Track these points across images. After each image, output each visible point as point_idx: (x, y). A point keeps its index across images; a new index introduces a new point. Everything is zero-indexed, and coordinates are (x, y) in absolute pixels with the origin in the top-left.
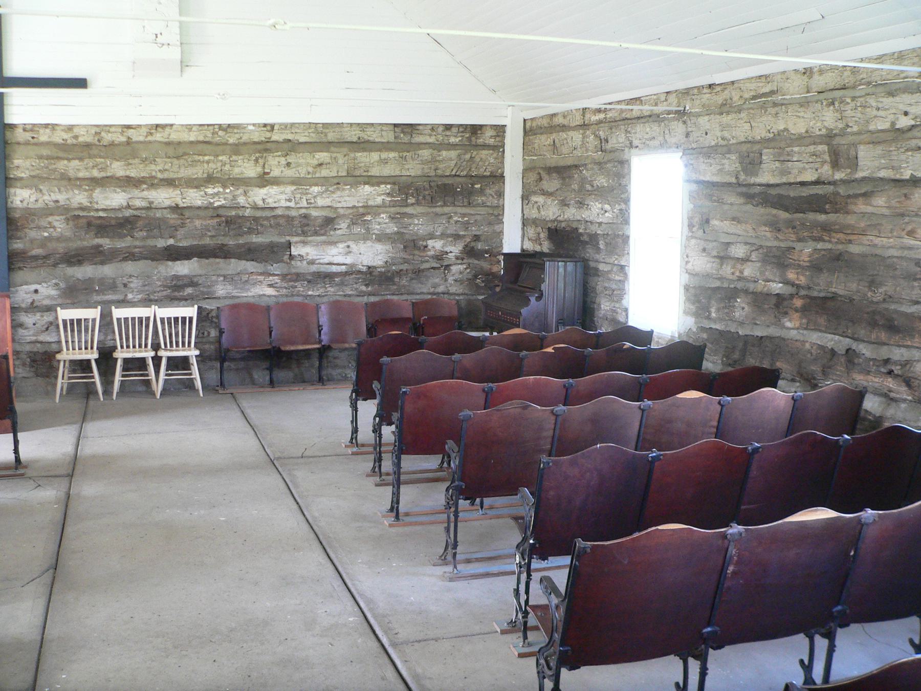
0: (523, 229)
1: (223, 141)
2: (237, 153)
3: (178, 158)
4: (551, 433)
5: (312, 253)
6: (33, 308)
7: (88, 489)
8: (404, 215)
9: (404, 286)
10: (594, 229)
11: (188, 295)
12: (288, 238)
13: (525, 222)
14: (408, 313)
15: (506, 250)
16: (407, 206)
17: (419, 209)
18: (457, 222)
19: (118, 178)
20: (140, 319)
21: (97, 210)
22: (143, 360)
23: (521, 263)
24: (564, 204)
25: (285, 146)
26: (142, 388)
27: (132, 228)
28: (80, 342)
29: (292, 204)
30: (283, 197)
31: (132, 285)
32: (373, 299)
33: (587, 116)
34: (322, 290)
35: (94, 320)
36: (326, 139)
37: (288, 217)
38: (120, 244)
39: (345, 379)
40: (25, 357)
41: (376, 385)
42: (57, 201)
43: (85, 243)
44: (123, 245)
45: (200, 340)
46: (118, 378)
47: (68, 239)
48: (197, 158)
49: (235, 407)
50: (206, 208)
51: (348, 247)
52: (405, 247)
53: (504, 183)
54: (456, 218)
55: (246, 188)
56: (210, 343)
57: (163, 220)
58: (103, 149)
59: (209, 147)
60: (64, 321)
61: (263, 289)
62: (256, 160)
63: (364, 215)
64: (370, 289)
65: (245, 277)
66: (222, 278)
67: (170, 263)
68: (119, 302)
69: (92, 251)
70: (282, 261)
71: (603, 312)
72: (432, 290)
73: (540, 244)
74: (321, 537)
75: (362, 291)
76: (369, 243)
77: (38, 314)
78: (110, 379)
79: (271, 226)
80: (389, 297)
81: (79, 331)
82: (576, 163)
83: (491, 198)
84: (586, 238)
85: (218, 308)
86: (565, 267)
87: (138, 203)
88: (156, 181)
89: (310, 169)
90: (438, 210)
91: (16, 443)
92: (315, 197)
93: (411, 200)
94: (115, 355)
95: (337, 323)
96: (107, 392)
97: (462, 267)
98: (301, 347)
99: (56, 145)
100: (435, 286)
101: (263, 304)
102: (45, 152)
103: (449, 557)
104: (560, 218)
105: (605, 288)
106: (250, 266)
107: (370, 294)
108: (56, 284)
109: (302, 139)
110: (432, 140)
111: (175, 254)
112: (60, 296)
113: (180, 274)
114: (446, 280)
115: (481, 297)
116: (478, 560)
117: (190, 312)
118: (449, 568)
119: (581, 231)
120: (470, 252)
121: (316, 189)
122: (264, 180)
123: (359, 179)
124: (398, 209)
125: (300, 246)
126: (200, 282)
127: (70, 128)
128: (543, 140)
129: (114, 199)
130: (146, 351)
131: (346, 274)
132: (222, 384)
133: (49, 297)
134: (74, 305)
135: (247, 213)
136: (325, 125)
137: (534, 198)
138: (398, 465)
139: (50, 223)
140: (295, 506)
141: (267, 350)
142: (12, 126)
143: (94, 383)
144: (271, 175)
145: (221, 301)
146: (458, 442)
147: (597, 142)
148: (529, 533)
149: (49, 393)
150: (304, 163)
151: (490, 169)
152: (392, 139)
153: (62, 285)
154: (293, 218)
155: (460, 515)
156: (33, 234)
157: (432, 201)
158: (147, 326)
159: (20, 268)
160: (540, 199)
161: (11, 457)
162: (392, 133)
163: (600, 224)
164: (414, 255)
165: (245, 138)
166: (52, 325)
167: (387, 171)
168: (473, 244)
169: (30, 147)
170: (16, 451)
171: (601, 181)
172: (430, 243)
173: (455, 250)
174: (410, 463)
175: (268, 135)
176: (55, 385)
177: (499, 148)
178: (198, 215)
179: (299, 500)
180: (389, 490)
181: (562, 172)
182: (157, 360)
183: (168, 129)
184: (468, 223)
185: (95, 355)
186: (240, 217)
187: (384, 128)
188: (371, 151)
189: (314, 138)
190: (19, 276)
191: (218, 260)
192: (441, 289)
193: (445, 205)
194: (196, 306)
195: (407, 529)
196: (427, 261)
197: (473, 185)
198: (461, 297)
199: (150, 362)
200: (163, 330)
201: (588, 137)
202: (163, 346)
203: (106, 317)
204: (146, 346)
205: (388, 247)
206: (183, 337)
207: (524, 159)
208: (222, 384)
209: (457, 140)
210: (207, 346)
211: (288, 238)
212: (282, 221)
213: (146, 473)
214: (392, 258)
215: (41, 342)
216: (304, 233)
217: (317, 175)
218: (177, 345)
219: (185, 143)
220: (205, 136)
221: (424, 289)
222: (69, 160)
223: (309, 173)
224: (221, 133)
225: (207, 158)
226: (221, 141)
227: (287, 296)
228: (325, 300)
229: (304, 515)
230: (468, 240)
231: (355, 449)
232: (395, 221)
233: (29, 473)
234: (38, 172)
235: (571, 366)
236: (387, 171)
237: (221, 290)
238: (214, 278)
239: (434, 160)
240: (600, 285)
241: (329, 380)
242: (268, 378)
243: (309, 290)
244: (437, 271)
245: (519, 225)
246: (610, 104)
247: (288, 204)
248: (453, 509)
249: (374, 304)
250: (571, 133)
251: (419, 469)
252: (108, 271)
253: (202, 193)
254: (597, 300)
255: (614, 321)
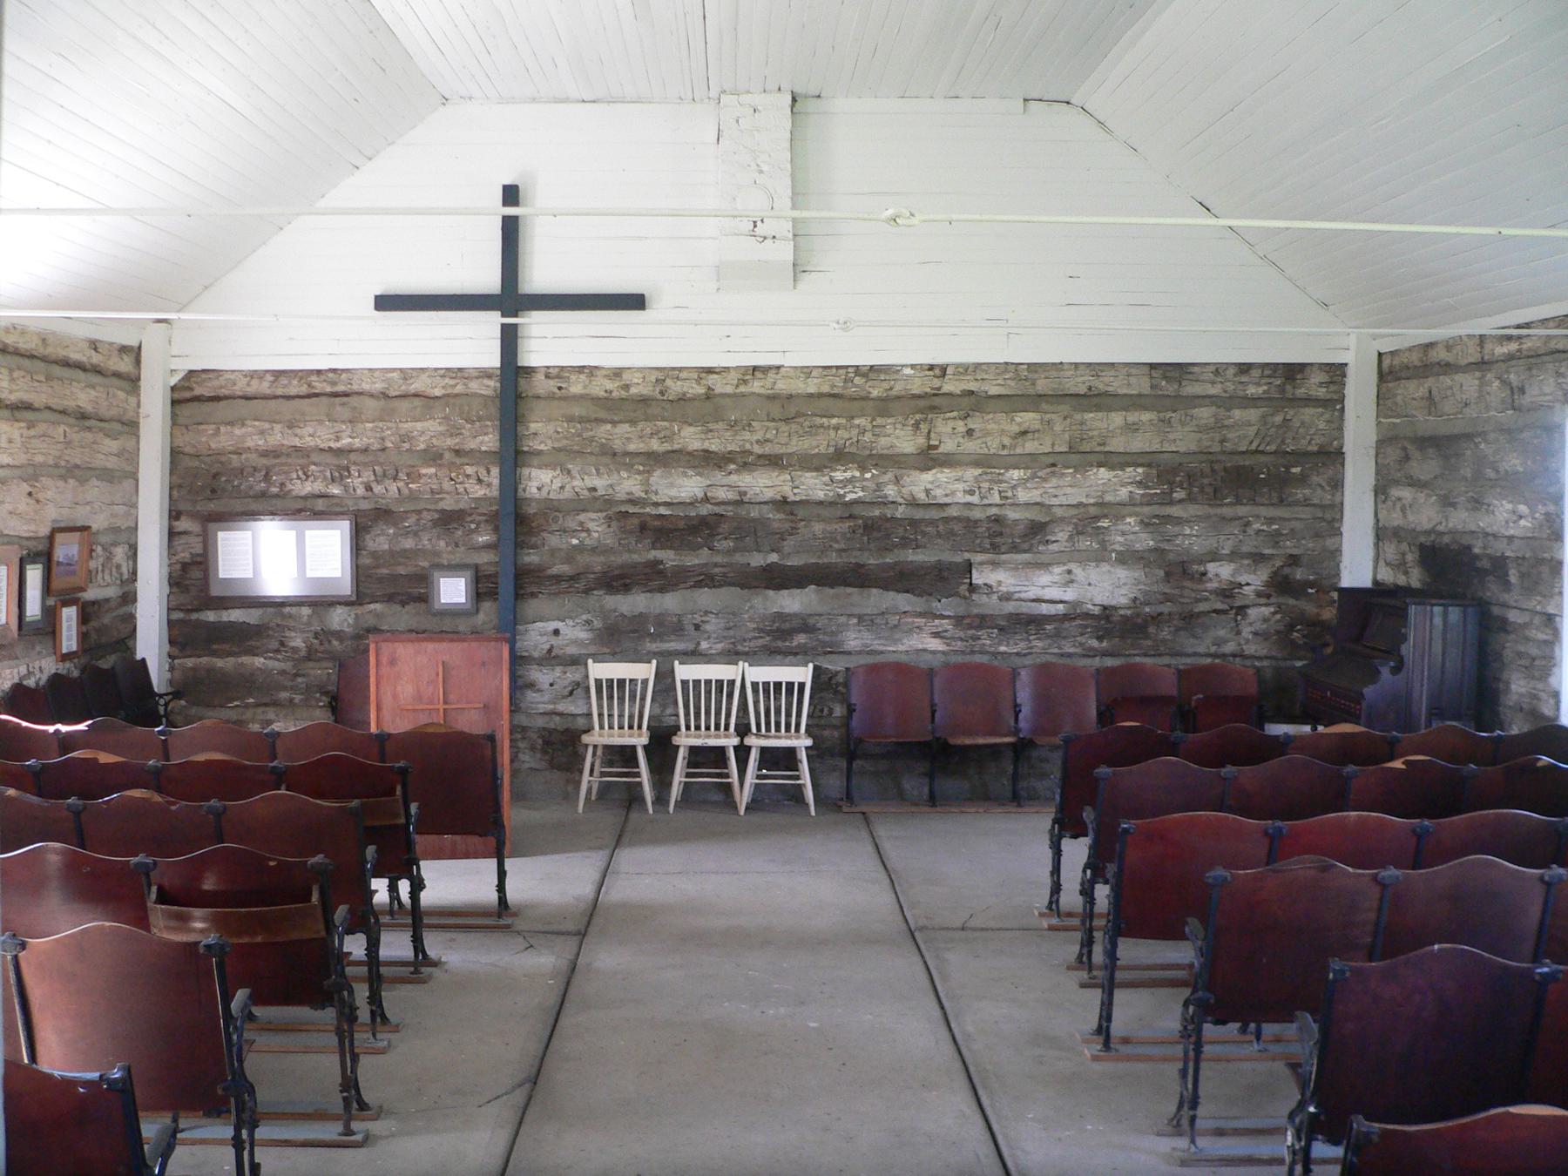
0: (1376, 545)
1: (863, 394)
2: (884, 413)
3: (786, 420)
4: (1372, 916)
5: (1000, 580)
6: (551, 658)
7: (605, 958)
8: (1168, 519)
9: (1164, 641)
10: (1499, 548)
11: (799, 646)
12: (967, 556)
13: (1381, 534)
14: (1169, 687)
15: (1346, 582)
16: (1172, 503)
17: (1193, 510)
18: (1259, 531)
19: (690, 454)
20: (720, 683)
21: (656, 504)
22: (722, 750)
23: (1375, 609)
24: (1447, 502)
25: (966, 401)
26: (718, 797)
27: (712, 535)
28: (621, 716)
29: (975, 499)
30: (960, 486)
31: (708, 627)
32: (1110, 662)
33: (1488, 346)
34: (1022, 645)
35: (645, 682)
36: (1034, 390)
37: (968, 519)
38: (696, 559)
39: (1049, 800)
40: (534, 736)
41: (1088, 815)
42: (594, 489)
43: (636, 558)
44: (697, 562)
45: (815, 721)
46: (678, 777)
47: (607, 551)
48: (818, 421)
49: (864, 834)
50: (832, 504)
51: (1069, 572)
52: (1167, 574)
53: (1343, 465)
54: (1257, 526)
55: (898, 472)
56: (835, 727)
57: (763, 522)
58: (668, 406)
59: (840, 403)
60: (598, 682)
61: (924, 641)
62: (916, 426)
63: (1097, 518)
64: (1105, 644)
65: (894, 620)
66: (855, 621)
67: (771, 593)
68: (685, 653)
69: (648, 570)
70: (957, 594)
71: (1515, 697)
72: (1213, 649)
73: (1406, 573)
74: (972, 1069)
75: (1091, 649)
76: (1105, 567)
77: (559, 669)
78: (670, 783)
79: (939, 535)
80: (1138, 659)
81: (621, 699)
82: (1469, 430)
83: (1319, 491)
84: (1485, 564)
85: (848, 669)
86: (1445, 615)
87: (722, 494)
88: (751, 459)
89: (1007, 441)
90: (1227, 511)
91: (502, 874)
92: (1014, 487)
93: (1179, 494)
94: (676, 740)
95: (1044, 700)
96: (661, 800)
97: (1266, 611)
98: (981, 741)
99: (596, 400)
100: (1219, 642)
101: (922, 665)
102: (577, 411)
103: (1185, 1123)
104: (1441, 528)
105: (1520, 655)
106: (903, 601)
107: (1105, 654)
108: (588, 622)
109: (994, 391)
110: (1213, 391)
111: (778, 578)
112: (593, 641)
113: (786, 611)
114: (1239, 633)
115: (1299, 664)
116: (1237, 1132)
117: (801, 674)
118: (1183, 1143)
119: (1476, 551)
120: (1281, 585)
121: (1016, 474)
122: (929, 458)
123: (1090, 458)
124: (1156, 510)
125: (987, 568)
126: (819, 625)
127: (617, 373)
128: (1413, 390)
129: (685, 487)
130: (726, 736)
131: (1065, 617)
132: (849, 797)
133: (575, 642)
134: (616, 656)
135: (900, 512)
136: (1032, 367)
137: (1395, 492)
138: (1111, 954)
139: (581, 524)
140: (937, 1013)
141: (925, 743)
142: (530, 371)
143: (640, 784)
144: (940, 450)
145: (853, 658)
146: (1204, 921)
147: (1505, 393)
148: (1308, 1094)
149: (570, 797)
150: (995, 431)
151: (1318, 440)
152: (1147, 391)
153: (597, 624)
154: (976, 522)
155: (1207, 1049)
156: (554, 541)
157: (1216, 496)
158: (730, 695)
159: (533, 595)
160: (1406, 493)
161: (493, 896)
162: (1147, 379)
163: (1511, 538)
164: (1183, 588)
165: (898, 388)
166: (579, 688)
167: (1138, 444)
168: (1287, 571)
169: (556, 403)
170: (501, 888)
171: (1513, 462)
172: (1212, 567)
173: (1255, 580)
174: (1133, 951)
175: (936, 383)
176: (579, 783)
177: (1334, 403)
178: (819, 516)
179: (944, 1001)
180: (1096, 996)
181: (1443, 445)
182: (742, 752)
183: (771, 375)
184: (1278, 533)
185: (645, 740)
186: (888, 520)
187: (1133, 371)
188: (1110, 409)
189: (1011, 388)
190: (532, 607)
191: (849, 590)
192: (1230, 648)
193: (1238, 502)
194: (811, 666)
195: (1122, 1067)
196: (1206, 599)
197: (1288, 468)
198: (1266, 663)
199: (732, 754)
200: (756, 703)
201: (1490, 384)
202: (754, 730)
203: (665, 677)
204: (727, 728)
205: (1138, 574)
206: (788, 715)
207: (1379, 424)
208: (849, 797)
209: (1260, 390)
210: (826, 733)
211: (967, 556)
212: (957, 527)
213: (698, 939)
214: (1146, 593)
215: (561, 714)
216: (995, 548)
217: (1019, 451)
218: (778, 729)
219: (798, 396)
220: (833, 386)
221: (1201, 648)
222: (614, 423)
223: (1004, 447)
224: (858, 380)
225: (834, 421)
226: (859, 393)
227: (963, 652)
228: (1028, 661)
229: (950, 1029)
230: (1278, 563)
231: (1055, 921)
232: (1151, 529)
233: (519, 924)
234: (565, 442)
235: (1433, 796)
236: (1138, 444)
237: (854, 639)
238: (842, 619)
239: (1219, 426)
240: (1510, 647)
241: (1030, 798)
242: (926, 790)
243: (1000, 644)
244: (1223, 617)
245: (1370, 539)
246: (1518, 327)
247: (969, 499)
248: (1193, 1039)
249: (1112, 671)
250: (1459, 377)
251: (1159, 961)
252: (670, 602)
253: (826, 479)
254: (1505, 676)
255: (1534, 714)
